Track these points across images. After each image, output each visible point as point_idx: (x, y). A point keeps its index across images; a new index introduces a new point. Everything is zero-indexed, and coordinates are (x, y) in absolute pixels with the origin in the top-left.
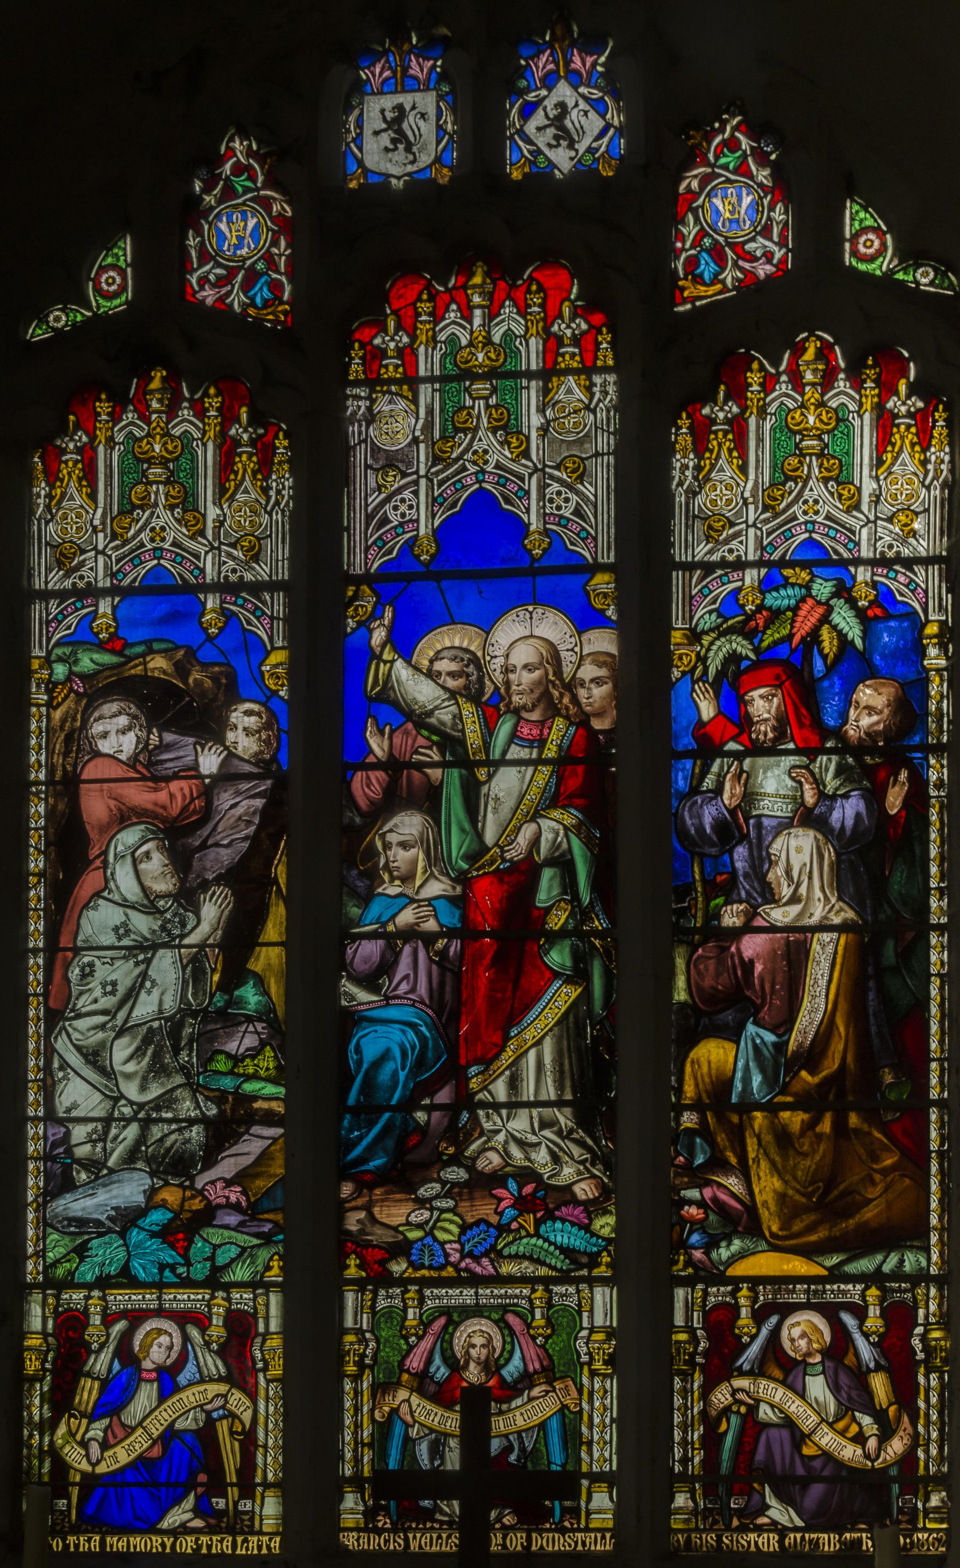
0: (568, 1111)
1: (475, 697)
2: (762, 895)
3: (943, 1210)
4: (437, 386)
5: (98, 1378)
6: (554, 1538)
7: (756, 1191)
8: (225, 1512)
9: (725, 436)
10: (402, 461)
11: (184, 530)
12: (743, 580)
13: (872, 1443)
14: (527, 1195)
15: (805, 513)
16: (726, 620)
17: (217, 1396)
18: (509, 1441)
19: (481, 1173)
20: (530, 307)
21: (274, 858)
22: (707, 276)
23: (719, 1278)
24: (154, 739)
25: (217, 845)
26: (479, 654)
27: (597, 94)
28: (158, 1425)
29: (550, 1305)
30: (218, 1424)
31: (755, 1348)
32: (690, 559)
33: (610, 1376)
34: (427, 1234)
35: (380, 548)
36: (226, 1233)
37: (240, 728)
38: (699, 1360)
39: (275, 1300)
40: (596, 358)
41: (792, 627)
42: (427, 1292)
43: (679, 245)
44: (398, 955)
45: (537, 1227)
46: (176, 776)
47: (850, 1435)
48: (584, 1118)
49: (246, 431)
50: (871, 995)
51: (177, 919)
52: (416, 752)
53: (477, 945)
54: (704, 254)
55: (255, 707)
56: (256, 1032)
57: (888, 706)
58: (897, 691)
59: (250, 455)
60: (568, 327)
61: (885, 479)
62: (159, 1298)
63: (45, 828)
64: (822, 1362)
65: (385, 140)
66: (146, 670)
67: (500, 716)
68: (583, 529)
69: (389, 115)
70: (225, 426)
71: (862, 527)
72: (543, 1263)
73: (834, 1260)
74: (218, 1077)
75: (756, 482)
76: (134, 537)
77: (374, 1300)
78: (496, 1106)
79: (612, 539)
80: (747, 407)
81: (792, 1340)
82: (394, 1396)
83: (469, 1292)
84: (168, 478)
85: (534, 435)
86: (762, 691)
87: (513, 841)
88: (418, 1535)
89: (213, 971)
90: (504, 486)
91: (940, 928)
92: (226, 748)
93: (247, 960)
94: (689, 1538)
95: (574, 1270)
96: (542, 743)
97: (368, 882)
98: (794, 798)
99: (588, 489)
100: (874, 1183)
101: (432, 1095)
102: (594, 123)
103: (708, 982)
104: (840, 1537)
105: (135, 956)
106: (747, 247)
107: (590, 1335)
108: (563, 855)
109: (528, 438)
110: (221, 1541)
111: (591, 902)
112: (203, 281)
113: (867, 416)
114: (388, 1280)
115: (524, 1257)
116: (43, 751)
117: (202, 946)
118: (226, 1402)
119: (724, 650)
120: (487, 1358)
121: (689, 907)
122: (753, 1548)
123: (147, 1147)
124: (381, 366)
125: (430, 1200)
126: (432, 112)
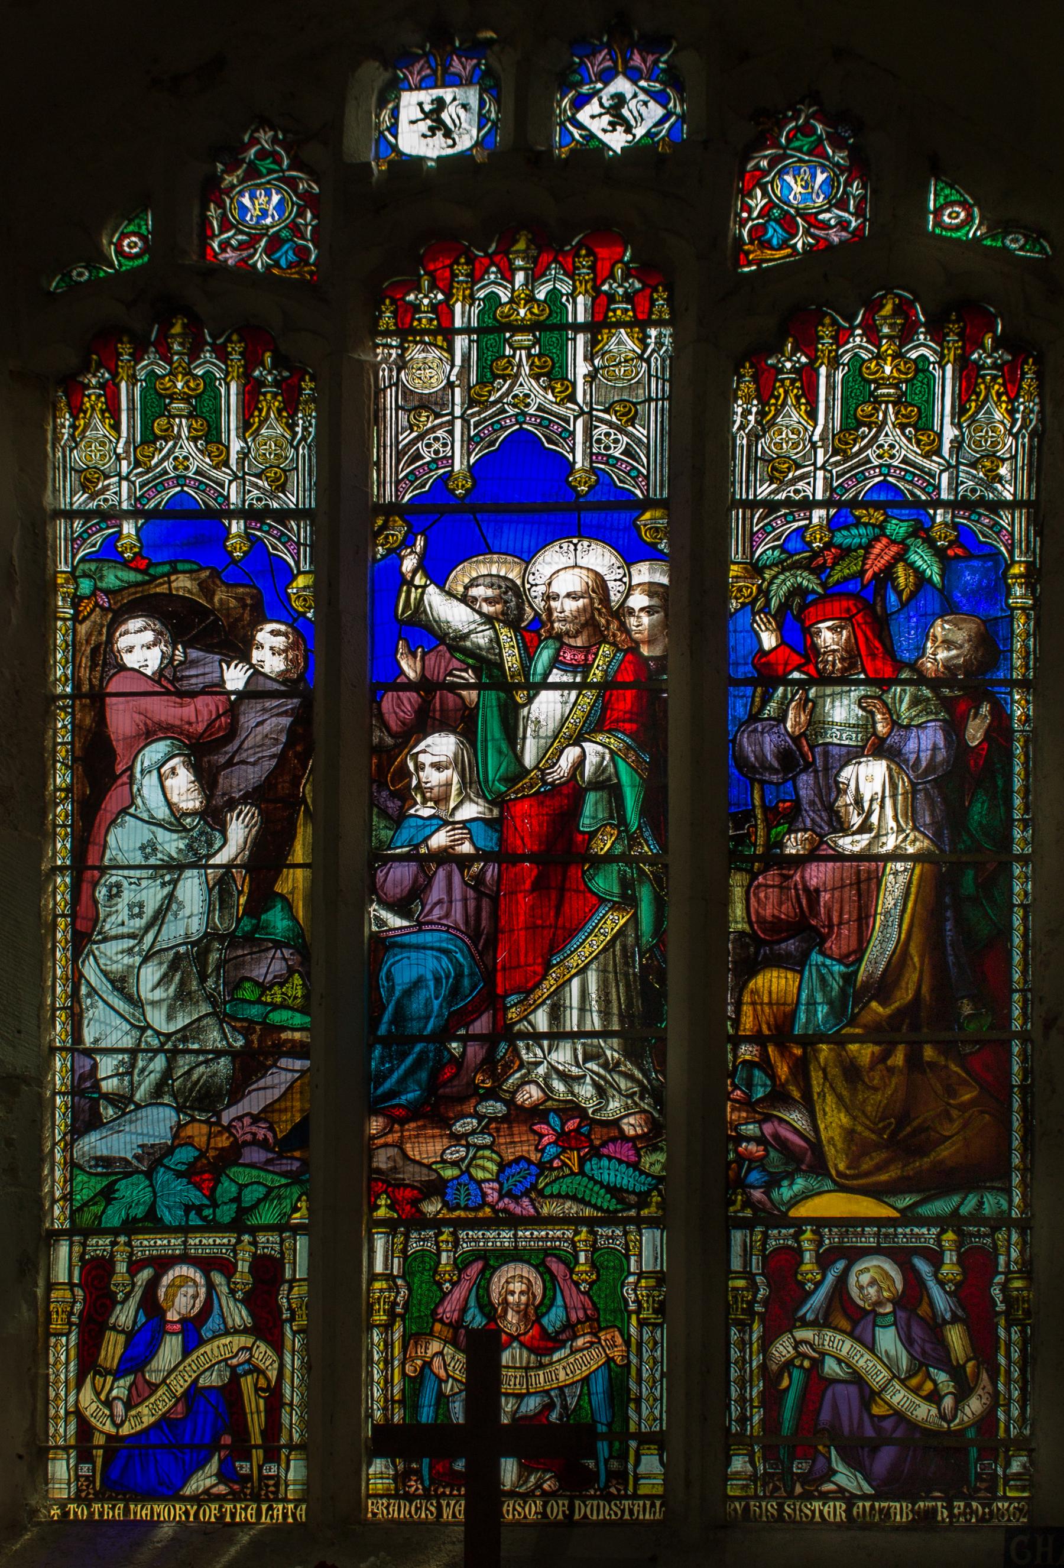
0: (615, 1042)
1: (513, 624)
2: (830, 823)
4: (475, 337)
5: (123, 1331)
6: (598, 1506)
7: (822, 1127)
8: (248, 1478)
10: (436, 404)
11: (207, 460)
12: (810, 518)
13: (948, 1402)
14: (570, 1131)
15: (879, 457)
16: (791, 556)
17: (242, 1349)
18: (551, 1398)
19: (521, 1107)
20: (578, 268)
21: (302, 777)
22: (775, 241)
23: (782, 1220)
24: (179, 655)
25: (243, 762)
26: (519, 582)
28: (182, 1382)
29: (594, 1248)
30: (242, 1380)
31: (818, 1299)
32: (751, 497)
33: (661, 1325)
34: (463, 1173)
35: (412, 482)
36: (255, 1172)
38: (758, 1308)
39: (302, 1243)
40: (651, 313)
41: (864, 564)
42: (462, 1235)
44: (430, 879)
45: (581, 1165)
46: (204, 692)
47: (924, 1393)
48: (631, 1052)
49: (270, 373)
50: (949, 926)
52: (451, 674)
53: (517, 869)
54: (773, 223)
55: (283, 628)
56: (284, 958)
57: (969, 641)
59: (275, 396)
60: (620, 286)
61: (968, 426)
62: (185, 1243)
63: (72, 743)
64: (894, 1312)
65: (423, 126)
66: (170, 589)
67: (541, 642)
68: (634, 468)
69: (427, 108)
71: (942, 471)
72: (588, 1204)
73: (907, 1201)
74: (246, 1006)
76: (157, 465)
78: (537, 1037)
79: (666, 478)
80: (817, 358)
81: (861, 1288)
82: (427, 1348)
83: (507, 1234)
86: (829, 623)
87: (555, 764)
88: (452, 1503)
89: (240, 893)
90: (547, 427)
91: (1024, 859)
92: (252, 666)
93: (275, 881)
94: (747, 1506)
95: (622, 1210)
96: (586, 668)
97: (399, 803)
98: (865, 727)
99: (639, 432)
100: (951, 1120)
101: (467, 1026)
102: (655, 111)
103: (768, 912)
104: (913, 1505)
105: (162, 876)
106: (821, 217)
107: (639, 1281)
108: (609, 779)
109: (574, 384)
110: (246, 1509)
111: (639, 827)
112: (225, 245)
115: (567, 1197)
117: (228, 867)
118: (252, 1356)
120: (527, 1305)
122: (817, 1518)
123: (174, 1081)
124: (413, 319)
125: (466, 1135)
126: (474, 103)
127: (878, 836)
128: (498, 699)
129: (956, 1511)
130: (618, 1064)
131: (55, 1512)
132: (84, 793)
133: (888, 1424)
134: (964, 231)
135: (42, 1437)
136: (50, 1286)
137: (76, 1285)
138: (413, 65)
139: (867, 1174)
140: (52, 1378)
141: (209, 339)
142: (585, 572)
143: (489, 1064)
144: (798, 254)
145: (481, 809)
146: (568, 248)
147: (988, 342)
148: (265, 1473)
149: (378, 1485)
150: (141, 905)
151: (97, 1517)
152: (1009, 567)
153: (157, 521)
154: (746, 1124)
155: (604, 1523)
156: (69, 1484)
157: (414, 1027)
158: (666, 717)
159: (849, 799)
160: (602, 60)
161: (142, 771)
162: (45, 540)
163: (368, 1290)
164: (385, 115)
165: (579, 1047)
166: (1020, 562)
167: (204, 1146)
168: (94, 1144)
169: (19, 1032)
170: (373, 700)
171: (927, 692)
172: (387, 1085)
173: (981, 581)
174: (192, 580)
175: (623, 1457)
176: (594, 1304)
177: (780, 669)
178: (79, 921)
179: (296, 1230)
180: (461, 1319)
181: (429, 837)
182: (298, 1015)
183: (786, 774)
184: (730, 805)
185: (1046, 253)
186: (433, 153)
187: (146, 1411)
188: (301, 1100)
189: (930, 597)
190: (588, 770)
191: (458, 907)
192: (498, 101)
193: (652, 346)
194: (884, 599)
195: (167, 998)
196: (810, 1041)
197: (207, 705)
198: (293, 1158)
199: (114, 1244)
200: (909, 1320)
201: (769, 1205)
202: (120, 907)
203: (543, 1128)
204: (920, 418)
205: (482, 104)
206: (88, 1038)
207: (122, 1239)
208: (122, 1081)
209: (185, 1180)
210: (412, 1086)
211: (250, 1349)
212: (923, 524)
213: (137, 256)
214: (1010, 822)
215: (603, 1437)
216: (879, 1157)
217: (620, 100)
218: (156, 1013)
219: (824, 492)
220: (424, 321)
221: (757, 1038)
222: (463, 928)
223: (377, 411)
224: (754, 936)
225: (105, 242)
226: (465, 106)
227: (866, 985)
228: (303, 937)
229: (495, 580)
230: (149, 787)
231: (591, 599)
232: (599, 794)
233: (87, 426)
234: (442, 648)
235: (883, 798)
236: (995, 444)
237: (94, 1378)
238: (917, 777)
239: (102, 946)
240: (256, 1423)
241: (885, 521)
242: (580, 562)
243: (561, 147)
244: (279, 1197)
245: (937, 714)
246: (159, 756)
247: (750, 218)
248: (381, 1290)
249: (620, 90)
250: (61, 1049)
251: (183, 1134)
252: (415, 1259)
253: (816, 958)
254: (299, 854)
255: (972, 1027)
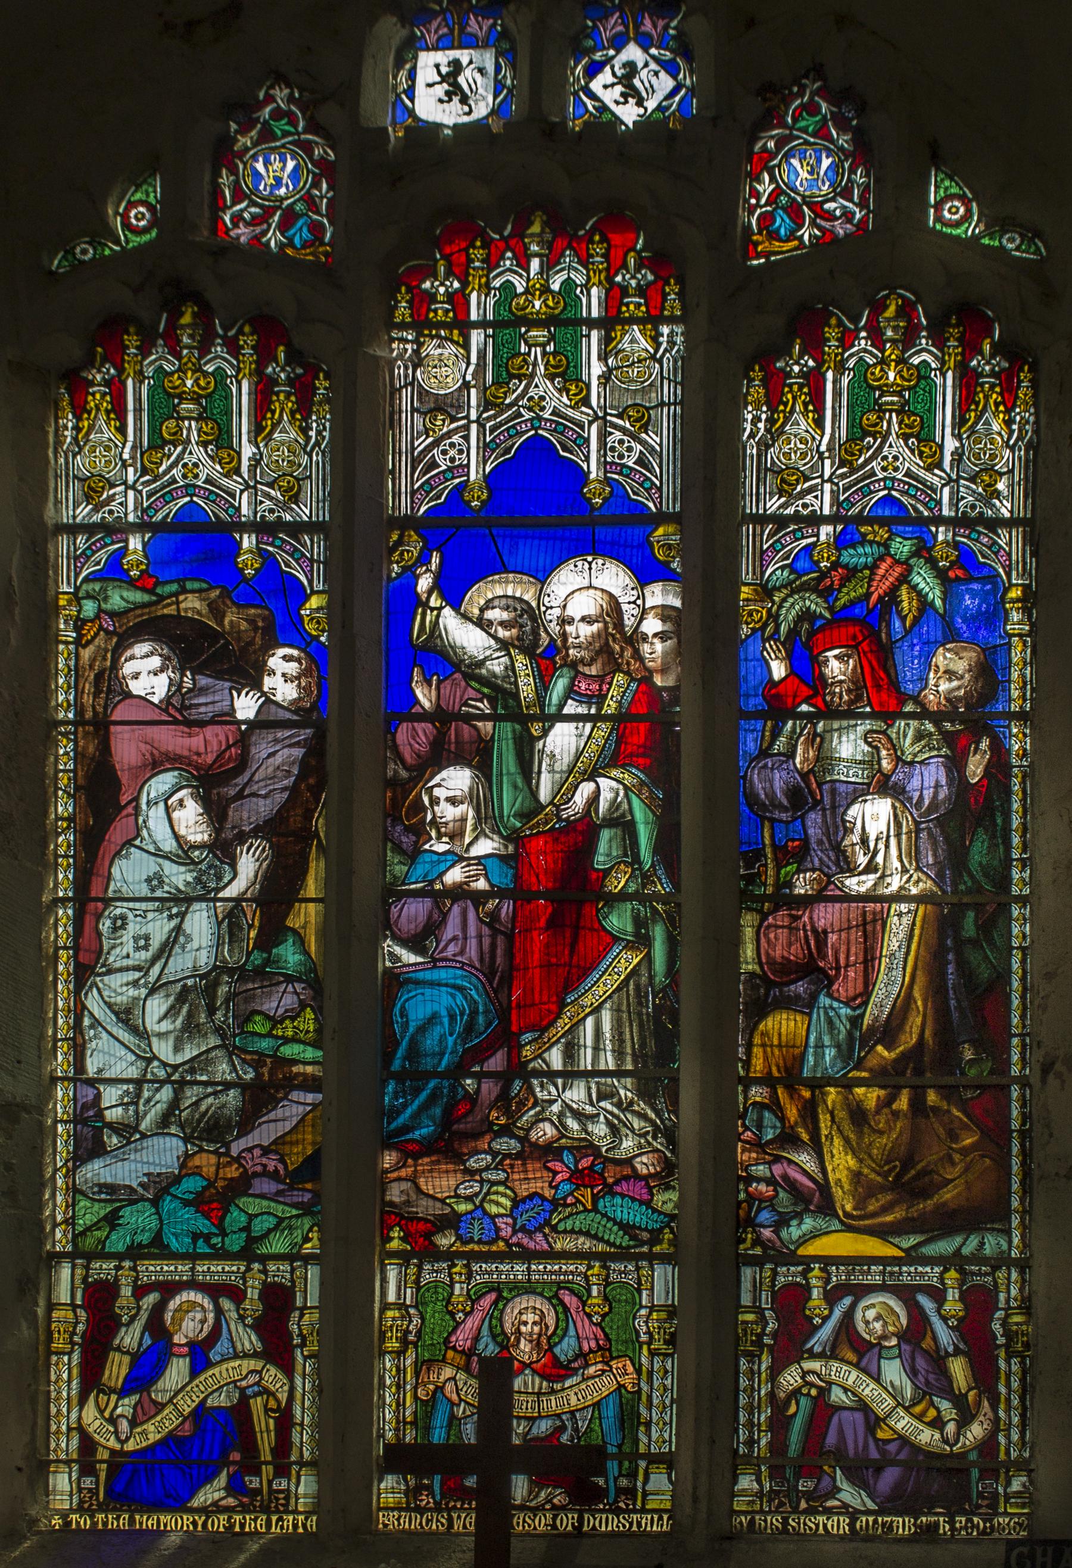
0: (629, 1082)
1: (529, 651)
2: (837, 864)
3: (1025, 1192)
5: (128, 1353)
7: (829, 1168)
8: (258, 1491)
9: (800, 389)
10: (452, 406)
11: (218, 467)
12: (817, 535)
13: (951, 1428)
14: (584, 1169)
15: (884, 469)
16: (799, 577)
17: (252, 1372)
18: (562, 1421)
19: (535, 1145)
20: (592, 256)
22: (782, 231)
23: (790, 1258)
25: (254, 795)
26: (534, 604)
27: (668, 55)
28: (189, 1402)
30: (252, 1401)
31: (826, 1332)
32: (761, 511)
33: (672, 1355)
34: (477, 1208)
35: (428, 493)
36: (265, 1203)
37: (279, 673)
38: (767, 1340)
39: (313, 1273)
40: (663, 308)
41: (869, 586)
42: (475, 1267)
43: (753, 201)
44: (445, 915)
45: (595, 1202)
46: (213, 722)
48: (645, 1092)
49: (283, 370)
50: (951, 969)
51: (212, 872)
54: (780, 212)
55: (295, 653)
56: (296, 993)
57: (970, 671)
58: (978, 657)
59: (288, 395)
60: (633, 277)
61: (968, 437)
62: (192, 1269)
63: (75, 771)
64: (899, 1345)
65: (440, 90)
68: (648, 479)
69: (444, 70)
70: (261, 364)
71: (943, 486)
72: (601, 1240)
74: (256, 1039)
75: (833, 435)
76: (165, 473)
77: (419, 1276)
78: (551, 1075)
79: (678, 490)
80: (824, 362)
81: (867, 1323)
82: (439, 1374)
83: (520, 1268)
84: (200, 415)
85: (594, 383)
86: (836, 652)
89: (251, 926)
90: (562, 433)
91: (1022, 900)
92: (264, 694)
93: (287, 915)
94: (752, 1520)
95: (635, 1247)
96: (600, 698)
97: (414, 838)
99: (652, 439)
100: (953, 1164)
101: (481, 1062)
102: (665, 83)
103: (778, 953)
105: (169, 909)
106: (827, 206)
107: (650, 1314)
108: (623, 815)
109: (588, 386)
111: (653, 865)
112: (237, 219)
113: (950, 374)
114: (437, 1255)
115: (580, 1232)
116: (72, 690)
117: (238, 900)
118: (261, 1379)
119: (797, 607)
120: (540, 1335)
121: (759, 874)
122: (821, 1530)
123: (181, 1111)
124: (429, 310)
125: (480, 1171)
126: (490, 68)
127: (883, 877)
128: (514, 731)
129: (958, 1525)
130: (631, 1103)
131: (57, 1522)
132: (87, 823)
133: (892, 1448)
134: (963, 228)
135: (43, 1451)
136: (51, 1307)
137: (79, 1306)
138: (430, 22)
139: (873, 1215)
140: (53, 1395)
141: (220, 331)
142: (599, 593)
143: (503, 1100)
144: (805, 247)
145: (496, 845)
146: (581, 233)
147: (987, 348)
148: (275, 1487)
149: (389, 1499)
150: (147, 938)
151: (100, 1526)
152: (1007, 590)
153: (165, 535)
154: (757, 1164)
155: (613, 1535)
156: (71, 1495)
157: (428, 1063)
158: (678, 751)
159: (855, 838)
160: (613, 25)
161: (148, 802)
162: (46, 559)
163: (381, 1318)
164: (403, 75)
165: (593, 1086)
166: (1017, 585)
167: (212, 1176)
168: (96, 1171)
169: (19, 1062)
170: (388, 731)
171: (930, 727)
172: (401, 1120)
173: (980, 605)
174: (201, 600)
175: (633, 1475)
176: (606, 1335)
177: (790, 701)
178: (81, 954)
179: (307, 1259)
180: (474, 1347)
181: (444, 872)
182: (310, 1049)
183: (795, 812)
184: (742, 843)
185: (1041, 254)
186: (449, 120)
187: (152, 1428)
188: (313, 1133)
189: (932, 623)
190: (603, 806)
191: (473, 943)
192: (514, 66)
193: (664, 345)
194: (889, 625)
195: (175, 1030)
196: (818, 1085)
197: (217, 735)
198: (304, 1190)
199: (118, 1268)
200: (913, 1352)
201: (778, 1244)
202: (124, 939)
203: (558, 1166)
204: (922, 428)
205: (498, 68)
206: (92, 1067)
207: (127, 1264)
208: (127, 1110)
209: (192, 1209)
210: (426, 1121)
211: (260, 1372)
212: (926, 542)
213: (145, 230)
214: (1008, 862)
215: (613, 1456)
216: (885, 1198)
217: (631, 68)
218: (163, 1044)
219: (831, 506)
220: (440, 312)
221: (767, 1081)
222: (477, 965)
223: (392, 414)
224: (764, 977)
225: (110, 212)
226: (481, 71)
227: (870, 1027)
228: (315, 971)
229: (510, 602)
230: (155, 820)
231: (606, 623)
232: (613, 831)
233: (91, 428)
234: (458, 676)
235: (888, 837)
236: (993, 457)
237: (97, 1396)
238: (920, 816)
239: (106, 978)
240: (266, 1442)
241: (889, 538)
242: (594, 583)
243: (574, 119)
244: (290, 1228)
245: (939, 749)
246: (167, 787)
247: (758, 205)
248: (394, 1319)
249: (632, 58)
250: (63, 1079)
251: (190, 1164)
252: (428, 1290)
253: (824, 1000)
254: (312, 887)
255: (973, 1072)
